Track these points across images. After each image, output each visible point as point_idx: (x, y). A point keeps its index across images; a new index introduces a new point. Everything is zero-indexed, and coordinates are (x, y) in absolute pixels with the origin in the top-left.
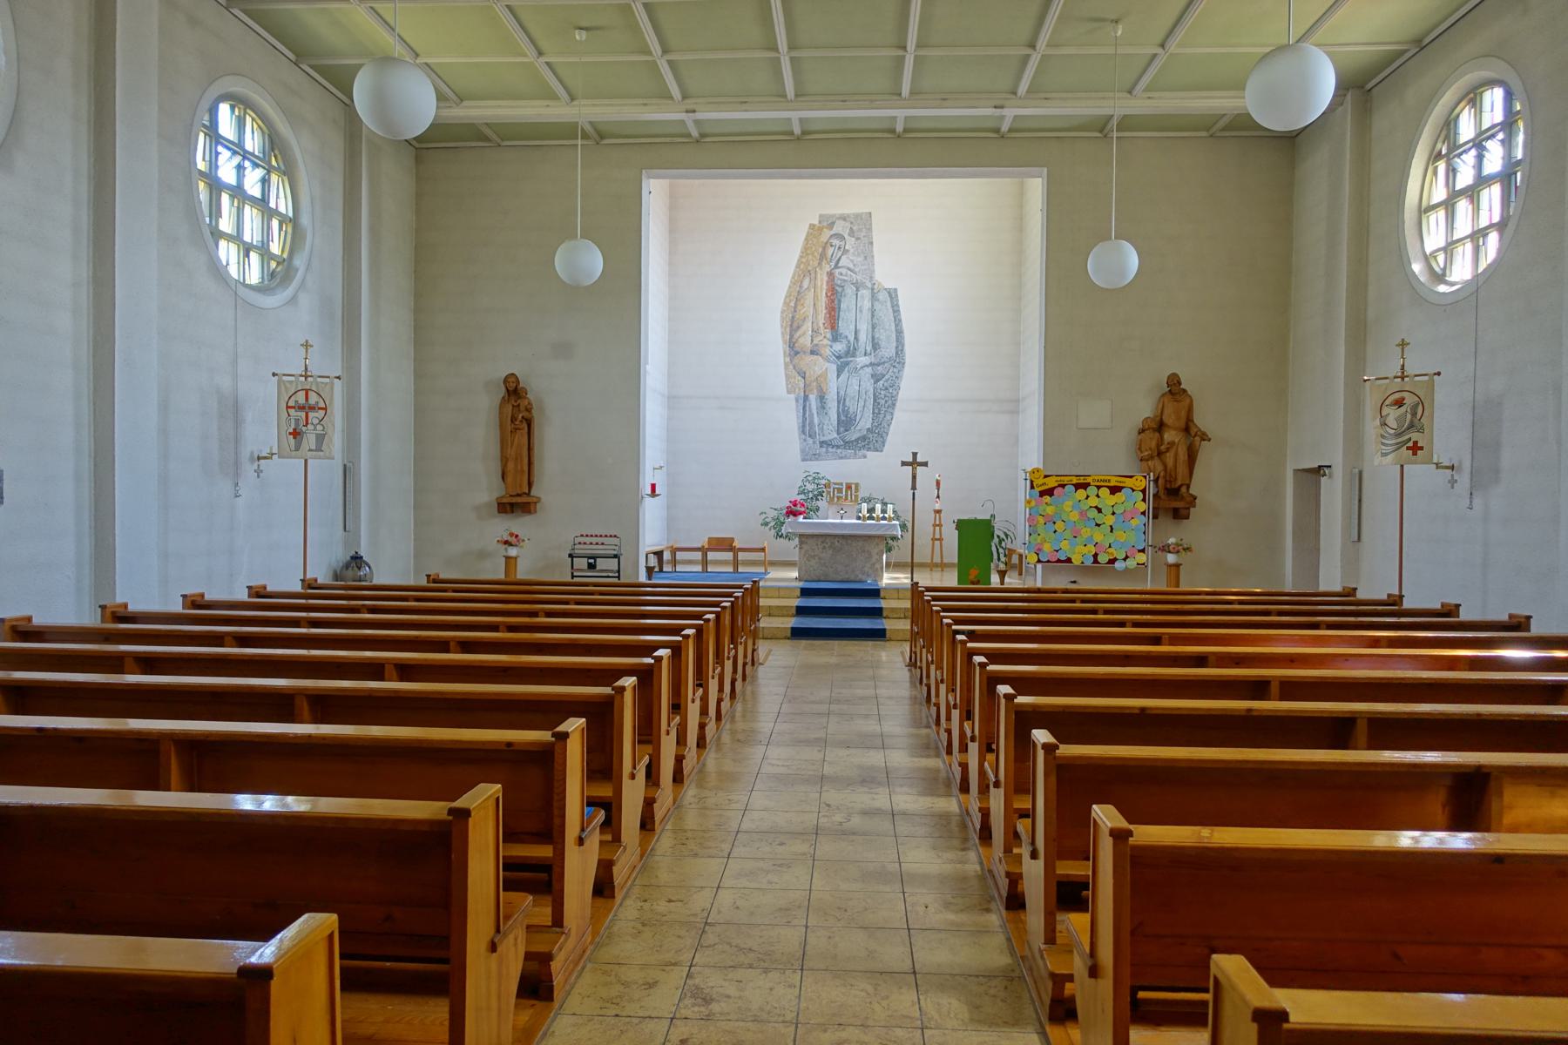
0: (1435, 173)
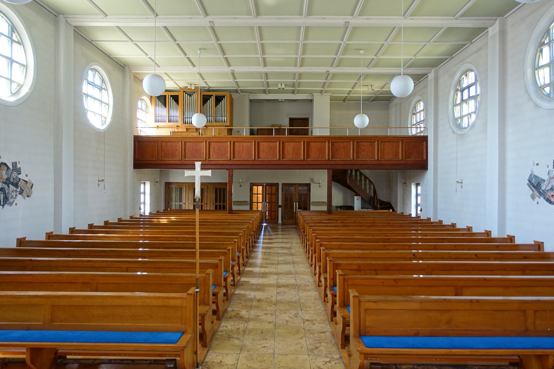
0: (457, 95)
